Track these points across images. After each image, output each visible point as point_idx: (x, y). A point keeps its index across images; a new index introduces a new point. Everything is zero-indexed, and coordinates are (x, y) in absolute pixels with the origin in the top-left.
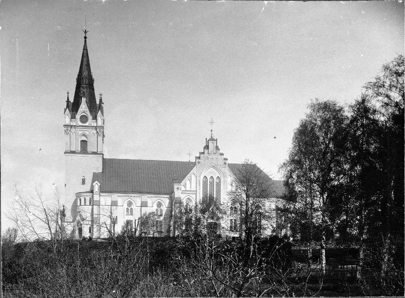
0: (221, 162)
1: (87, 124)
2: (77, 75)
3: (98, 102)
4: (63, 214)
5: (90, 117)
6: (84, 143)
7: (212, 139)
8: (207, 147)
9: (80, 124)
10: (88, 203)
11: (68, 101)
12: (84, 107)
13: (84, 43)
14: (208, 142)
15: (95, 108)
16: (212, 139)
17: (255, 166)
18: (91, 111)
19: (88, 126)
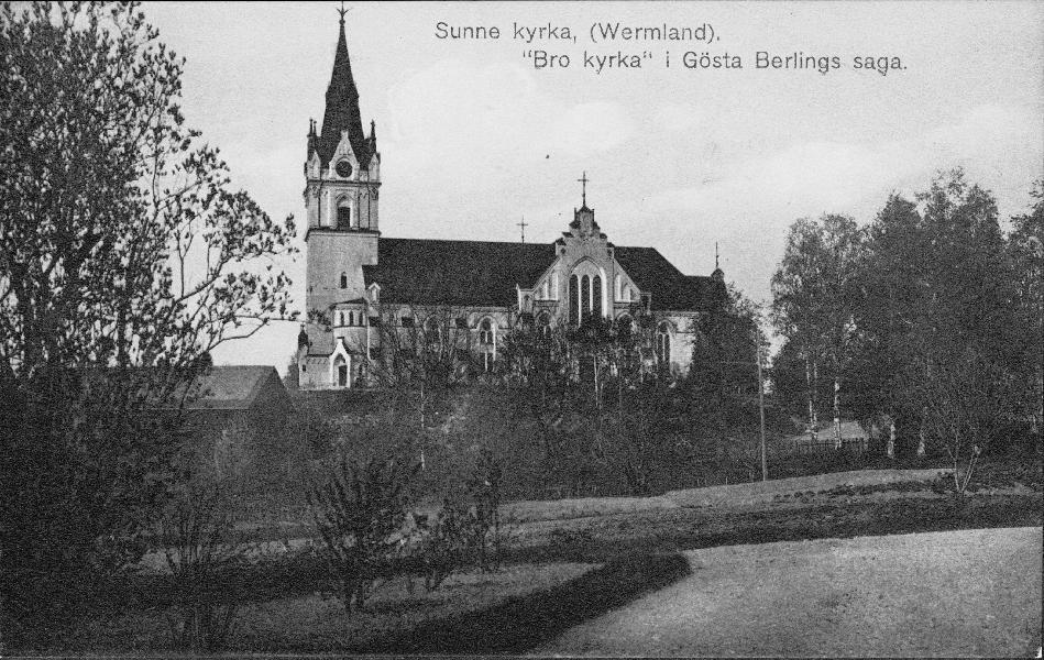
0: (602, 250)
1: (347, 179)
2: (331, 70)
3: (575, 570)
4: (304, 370)
5: (355, 165)
6: (343, 213)
7: (584, 209)
8: (575, 225)
9: (339, 178)
10: (356, 322)
11: (312, 134)
12: (345, 146)
13: (338, 36)
14: (577, 214)
15: (366, 150)
16: (584, 209)
17: (652, 249)
18: (358, 156)
19: (351, 182)
